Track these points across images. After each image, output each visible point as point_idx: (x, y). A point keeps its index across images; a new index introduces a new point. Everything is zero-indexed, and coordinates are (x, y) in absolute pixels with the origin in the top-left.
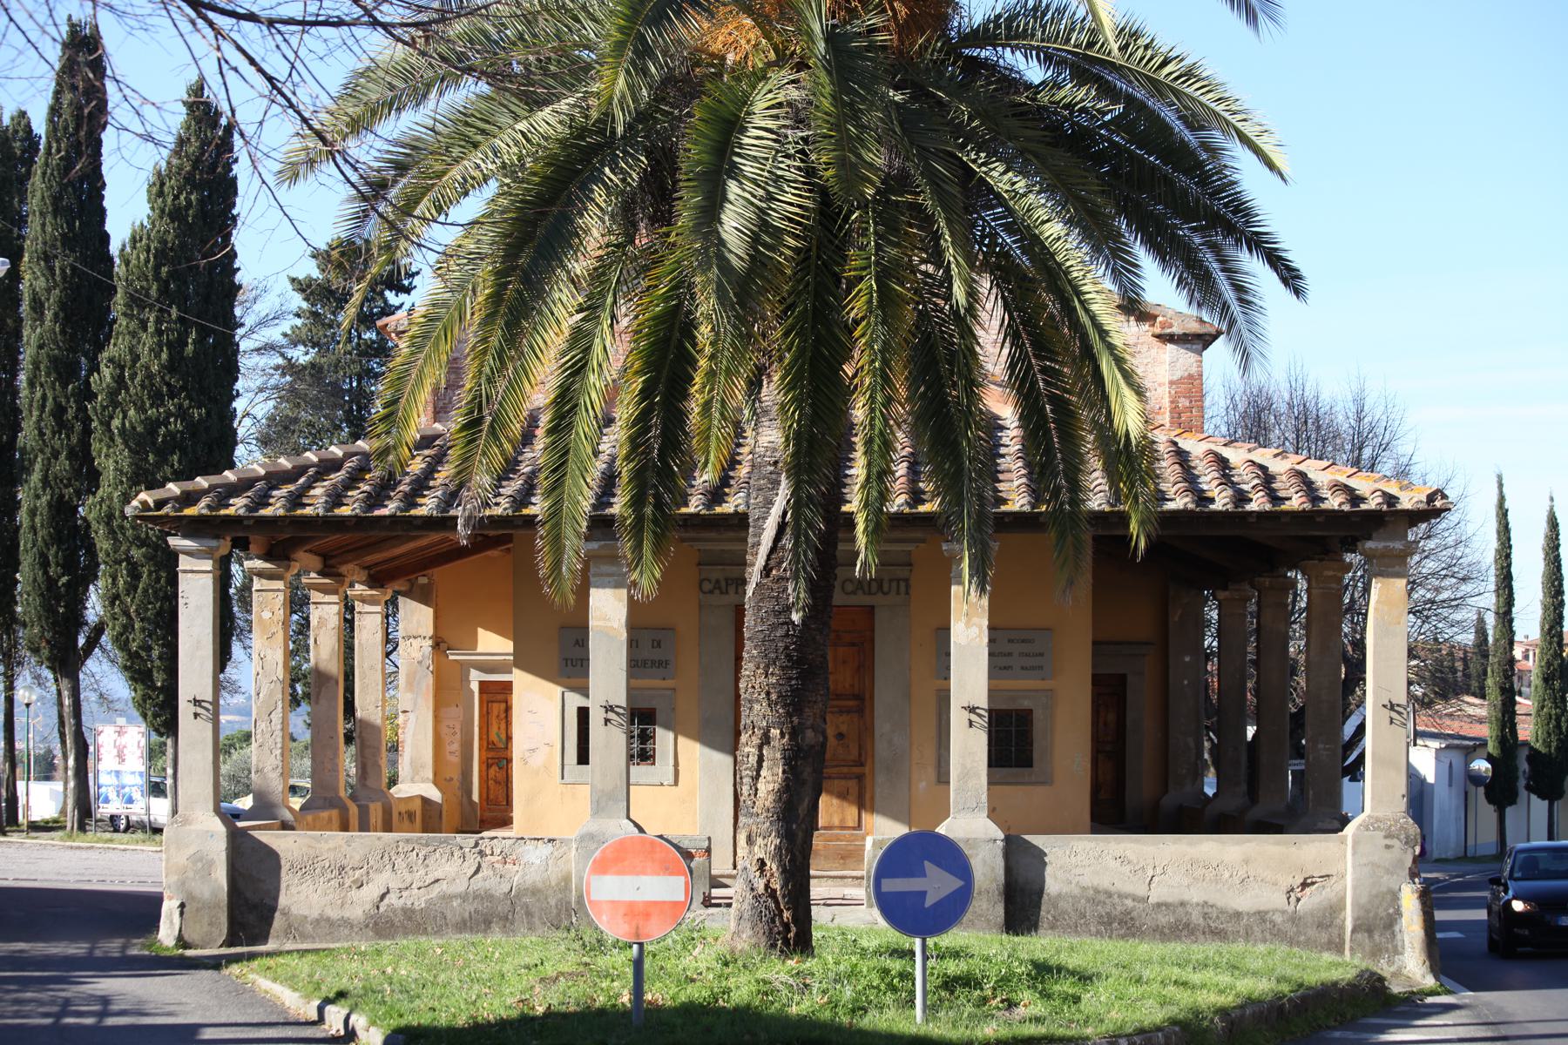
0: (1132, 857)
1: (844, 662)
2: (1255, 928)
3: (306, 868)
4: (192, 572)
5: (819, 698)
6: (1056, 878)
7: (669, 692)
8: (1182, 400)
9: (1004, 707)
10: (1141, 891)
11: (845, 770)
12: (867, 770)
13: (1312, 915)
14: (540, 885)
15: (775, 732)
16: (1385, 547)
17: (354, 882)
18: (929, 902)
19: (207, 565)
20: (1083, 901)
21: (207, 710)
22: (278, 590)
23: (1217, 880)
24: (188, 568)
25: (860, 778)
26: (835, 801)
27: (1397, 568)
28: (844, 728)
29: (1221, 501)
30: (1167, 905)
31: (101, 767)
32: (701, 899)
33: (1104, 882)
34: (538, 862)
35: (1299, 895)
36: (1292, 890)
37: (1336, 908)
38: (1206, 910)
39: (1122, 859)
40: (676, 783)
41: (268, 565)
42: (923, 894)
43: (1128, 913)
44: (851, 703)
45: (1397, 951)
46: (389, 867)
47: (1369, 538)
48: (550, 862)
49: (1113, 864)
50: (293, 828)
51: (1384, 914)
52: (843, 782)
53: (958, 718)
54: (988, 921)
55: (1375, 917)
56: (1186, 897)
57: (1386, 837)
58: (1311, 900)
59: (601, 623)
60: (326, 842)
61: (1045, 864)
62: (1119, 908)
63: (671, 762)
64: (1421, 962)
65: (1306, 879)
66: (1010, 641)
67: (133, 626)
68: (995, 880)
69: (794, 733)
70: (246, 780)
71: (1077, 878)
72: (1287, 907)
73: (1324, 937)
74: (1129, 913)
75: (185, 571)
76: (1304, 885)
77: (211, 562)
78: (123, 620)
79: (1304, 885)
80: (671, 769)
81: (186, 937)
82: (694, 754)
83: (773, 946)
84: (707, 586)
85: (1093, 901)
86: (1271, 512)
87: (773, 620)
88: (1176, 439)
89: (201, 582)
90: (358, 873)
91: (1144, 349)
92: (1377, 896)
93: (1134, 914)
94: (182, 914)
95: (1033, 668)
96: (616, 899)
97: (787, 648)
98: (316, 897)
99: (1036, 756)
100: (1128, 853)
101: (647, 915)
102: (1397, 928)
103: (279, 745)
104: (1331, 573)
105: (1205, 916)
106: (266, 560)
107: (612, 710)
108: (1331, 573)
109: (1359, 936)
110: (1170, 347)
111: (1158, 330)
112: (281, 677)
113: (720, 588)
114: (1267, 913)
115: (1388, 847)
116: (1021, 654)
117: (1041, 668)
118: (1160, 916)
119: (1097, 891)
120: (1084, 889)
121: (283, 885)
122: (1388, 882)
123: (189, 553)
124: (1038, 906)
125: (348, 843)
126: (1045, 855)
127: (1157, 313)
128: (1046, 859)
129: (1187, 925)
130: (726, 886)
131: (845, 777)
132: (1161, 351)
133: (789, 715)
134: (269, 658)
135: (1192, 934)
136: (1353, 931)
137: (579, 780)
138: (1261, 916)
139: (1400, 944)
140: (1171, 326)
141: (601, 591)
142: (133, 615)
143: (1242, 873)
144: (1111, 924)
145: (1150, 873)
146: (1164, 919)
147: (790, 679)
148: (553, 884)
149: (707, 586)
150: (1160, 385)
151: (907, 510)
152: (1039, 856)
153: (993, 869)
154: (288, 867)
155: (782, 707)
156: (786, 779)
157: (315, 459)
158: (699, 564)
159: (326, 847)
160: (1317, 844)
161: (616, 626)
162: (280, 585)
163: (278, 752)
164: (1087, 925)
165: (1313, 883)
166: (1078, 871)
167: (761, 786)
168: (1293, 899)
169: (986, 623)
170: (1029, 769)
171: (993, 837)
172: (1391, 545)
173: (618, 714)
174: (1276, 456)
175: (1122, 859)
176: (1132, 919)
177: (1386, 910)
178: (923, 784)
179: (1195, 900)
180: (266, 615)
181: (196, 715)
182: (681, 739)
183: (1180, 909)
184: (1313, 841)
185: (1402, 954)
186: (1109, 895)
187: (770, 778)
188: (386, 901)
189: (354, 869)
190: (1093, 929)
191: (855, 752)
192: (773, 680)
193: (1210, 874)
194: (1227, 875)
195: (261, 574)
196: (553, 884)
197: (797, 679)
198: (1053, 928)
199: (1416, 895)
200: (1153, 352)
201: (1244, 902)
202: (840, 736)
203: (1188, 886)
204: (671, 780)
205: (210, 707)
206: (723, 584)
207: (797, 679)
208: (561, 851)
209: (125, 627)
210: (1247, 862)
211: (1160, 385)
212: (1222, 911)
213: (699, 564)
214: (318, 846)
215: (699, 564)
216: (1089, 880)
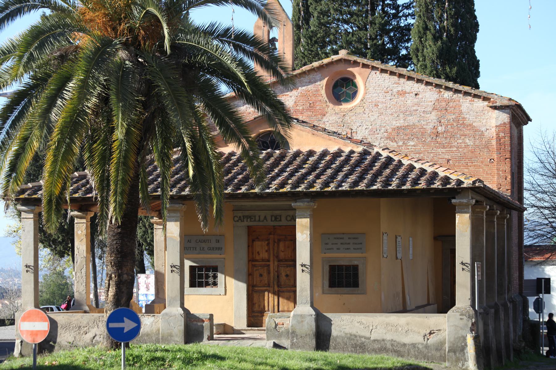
0: (364, 322)
1: (288, 247)
2: (411, 350)
3: (67, 327)
4: (26, 218)
5: (129, 264)
6: (336, 330)
7: (223, 259)
8: (501, 133)
9: (347, 264)
10: (368, 335)
11: (289, 289)
13: (433, 345)
14: (149, 332)
15: (113, 275)
16: (460, 202)
17: (84, 332)
18: (125, 331)
19: (31, 216)
20: (346, 339)
21: (32, 269)
22: (84, 223)
23: (397, 331)
24: (25, 217)
26: (285, 301)
27: (465, 210)
28: (288, 273)
30: (377, 341)
31: (140, 292)
32: (207, 337)
33: (354, 332)
34: (149, 324)
35: (428, 337)
36: (426, 335)
37: (442, 343)
38: (392, 343)
39: (360, 323)
40: (225, 294)
41: (79, 214)
42: (123, 328)
43: (363, 343)
44: (291, 263)
45: (466, 360)
46: (96, 326)
47: (454, 198)
48: (153, 324)
50: (88, 313)
51: (460, 345)
52: (288, 293)
53: (458, 267)
54: (309, 346)
55: (457, 346)
56: (385, 338)
57: (460, 315)
58: (433, 340)
59: (171, 235)
60: (74, 317)
61: (332, 324)
62: (359, 342)
63: (224, 286)
64: (474, 365)
65: (431, 331)
66: (349, 238)
67: (148, 232)
68: (312, 330)
69: (119, 276)
71: (344, 330)
72: (423, 342)
73: (438, 354)
74: (363, 344)
75: (23, 218)
76: (430, 333)
77: (33, 215)
78: (144, 229)
79: (430, 333)
80: (224, 289)
81: (23, 353)
82: (232, 283)
83: (112, 347)
84: (236, 219)
85: (349, 339)
86: (411, 189)
87: (113, 238)
88: (401, 160)
89: (30, 222)
90: (85, 328)
91: (486, 112)
92: (457, 338)
93: (365, 344)
94: (21, 345)
95: (358, 249)
96: (28, 329)
97: (117, 247)
98: (70, 337)
99: (360, 283)
100: (363, 320)
101: (37, 335)
102: (465, 351)
103: (85, 282)
104: (479, 210)
105: (392, 345)
106: (79, 212)
107: (464, 265)
108: (479, 210)
109: (451, 354)
110: (496, 111)
111: (491, 104)
112: (85, 256)
113: (241, 220)
114: (416, 344)
115: (461, 319)
116: (353, 243)
118: (375, 345)
119: (351, 335)
120: (346, 334)
121: (59, 334)
122: (462, 333)
123: (25, 211)
124: (329, 341)
125: (82, 318)
126: (332, 321)
127: (490, 97)
128: (332, 322)
129: (385, 349)
130: (244, 334)
131: (289, 291)
132: (493, 113)
133: (118, 270)
134: (81, 248)
135: (387, 352)
136: (448, 352)
137: (190, 293)
138: (414, 345)
139: (467, 357)
140: (496, 102)
141: (170, 223)
142: (147, 227)
143: (406, 329)
144: (356, 348)
145: (371, 328)
146: (376, 346)
147: (118, 258)
148: (154, 332)
149: (236, 219)
150: (493, 127)
151: (275, 191)
152: (329, 321)
153: (311, 326)
154: (60, 327)
155: (115, 267)
156: (116, 291)
157: (77, 175)
158: (233, 210)
159: (74, 319)
160: (435, 317)
161: (176, 236)
162: (84, 221)
163: (84, 284)
164: (347, 348)
165: (434, 333)
166: (344, 327)
167: (109, 293)
168: (426, 339)
169: (309, 233)
170: (357, 288)
171: (311, 314)
172: (462, 201)
173: (177, 268)
174: (430, 166)
175: (360, 323)
176: (364, 346)
177: (461, 344)
178: (317, 294)
179: (388, 339)
180: (80, 232)
181: (463, 269)
182: (227, 277)
183: (383, 342)
184: (434, 316)
185: (468, 361)
186: (356, 336)
187: (112, 291)
188: (95, 339)
189: (84, 327)
190: (350, 350)
192: (112, 258)
193: (394, 329)
194: (400, 329)
195: (78, 217)
196: (154, 332)
197: (120, 258)
198: (335, 349)
199: (472, 338)
200: (490, 113)
201: (407, 340)
202: (287, 276)
203: (386, 333)
204: (224, 293)
205: (33, 268)
206: (242, 218)
207: (120, 258)
208: (157, 319)
209: (144, 232)
210: (408, 324)
211: (493, 127)
212: (399, 343)
213: (233, 210)
214: (71, 319)
215: (233, 210)
216: (348, 330)
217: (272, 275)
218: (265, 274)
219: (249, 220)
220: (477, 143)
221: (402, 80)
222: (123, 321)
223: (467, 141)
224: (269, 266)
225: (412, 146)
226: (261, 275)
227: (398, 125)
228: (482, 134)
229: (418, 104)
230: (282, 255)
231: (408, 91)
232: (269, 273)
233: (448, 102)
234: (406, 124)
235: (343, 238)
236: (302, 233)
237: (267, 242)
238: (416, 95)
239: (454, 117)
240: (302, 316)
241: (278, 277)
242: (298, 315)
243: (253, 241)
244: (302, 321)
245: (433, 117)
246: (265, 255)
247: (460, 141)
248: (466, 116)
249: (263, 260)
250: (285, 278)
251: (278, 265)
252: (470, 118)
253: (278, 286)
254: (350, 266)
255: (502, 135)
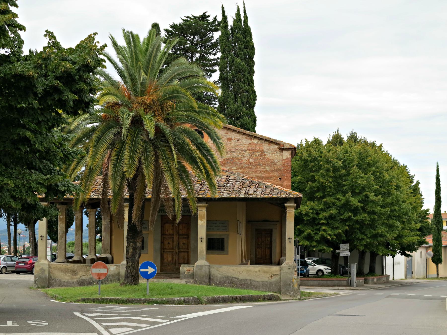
12: (189, 251)
25: (188, 252)
28: (184, 242)
29: (49, 241)
42: (148, 272)
44: (186, 236)
47: (286, 203)
49: (231, 271)
66: (220, 223)
70: (375, 249)
95: (224, 229)
101: (101, 275)
115: (289, 269)
117: (226, 229)
149: (185, 211)
166: (224, 272)
172: (290, 205)
191: (186, 247)
202: (184, 244)
217: (175, 243)
218: (171, 243)
219: (162, 212)
220: (272, 169)
221: (230, 132)
222: (148, 268)
223: (267, 168)
224: (173, 237)
225: (235, 169)
226: (169, 243)
227: (227, 157)
228: (275, 164)
229: (238, 146)
230: (181, 232)
231: (233, 138)
232: (173, 242)
233: (256, 145)
234: (232, 157)
235: (216, 223)
236: (201, 220)
237: (172, 225)
238: (238, 140)
239: (259, 153)
240: (201, 266)
241: (178, 244)
242: (199, 266)
243: (164, 224)
244: (201, 269)
245: (247, 153)
246: (171, 232)
247: (262, 168)
248: (266, 154)
249: (170, 235)
250: (182, 244)
251: (179, 237)
252: (268, 155)
253: (178, 249)
254: (219, 239)
255: (286, 164)
